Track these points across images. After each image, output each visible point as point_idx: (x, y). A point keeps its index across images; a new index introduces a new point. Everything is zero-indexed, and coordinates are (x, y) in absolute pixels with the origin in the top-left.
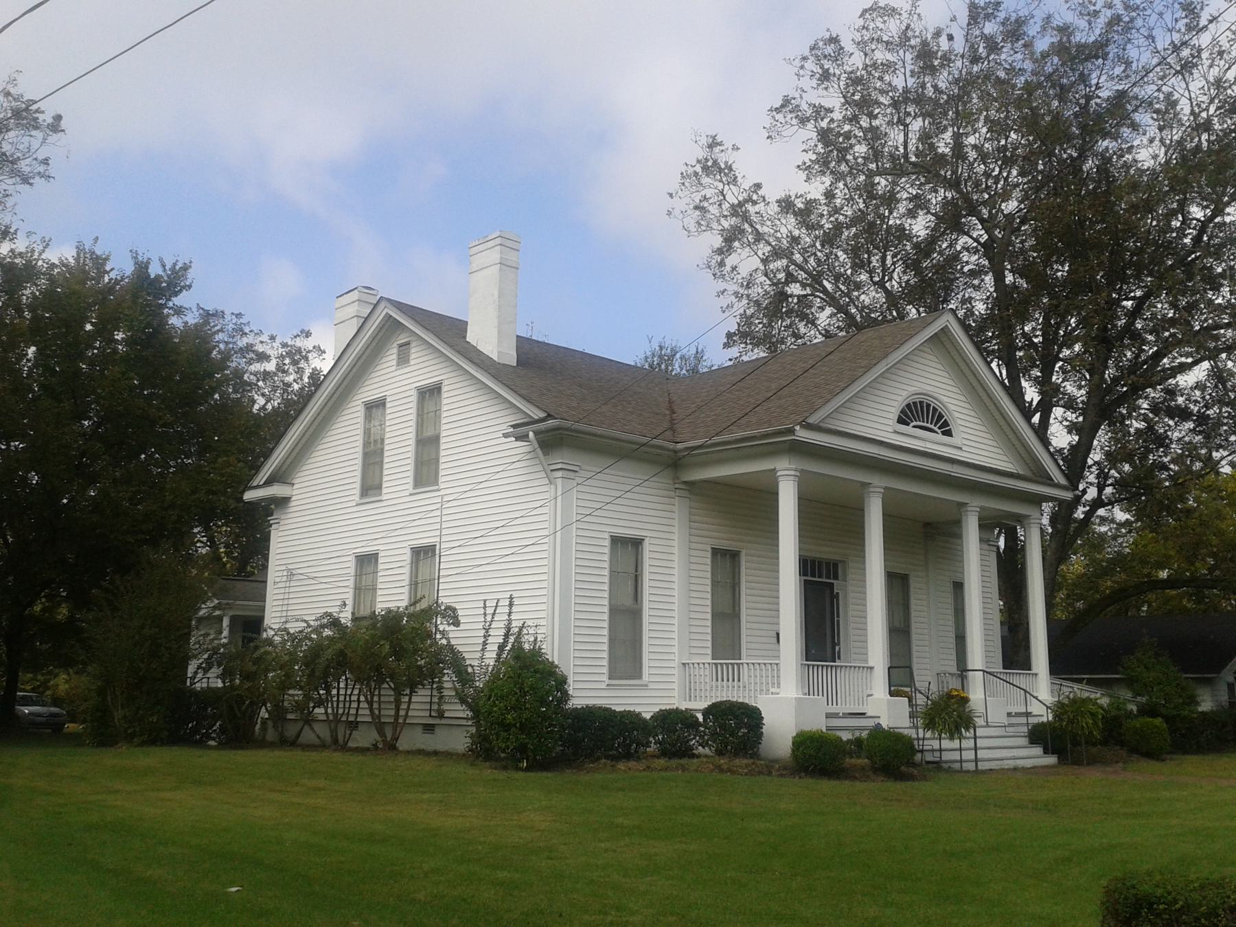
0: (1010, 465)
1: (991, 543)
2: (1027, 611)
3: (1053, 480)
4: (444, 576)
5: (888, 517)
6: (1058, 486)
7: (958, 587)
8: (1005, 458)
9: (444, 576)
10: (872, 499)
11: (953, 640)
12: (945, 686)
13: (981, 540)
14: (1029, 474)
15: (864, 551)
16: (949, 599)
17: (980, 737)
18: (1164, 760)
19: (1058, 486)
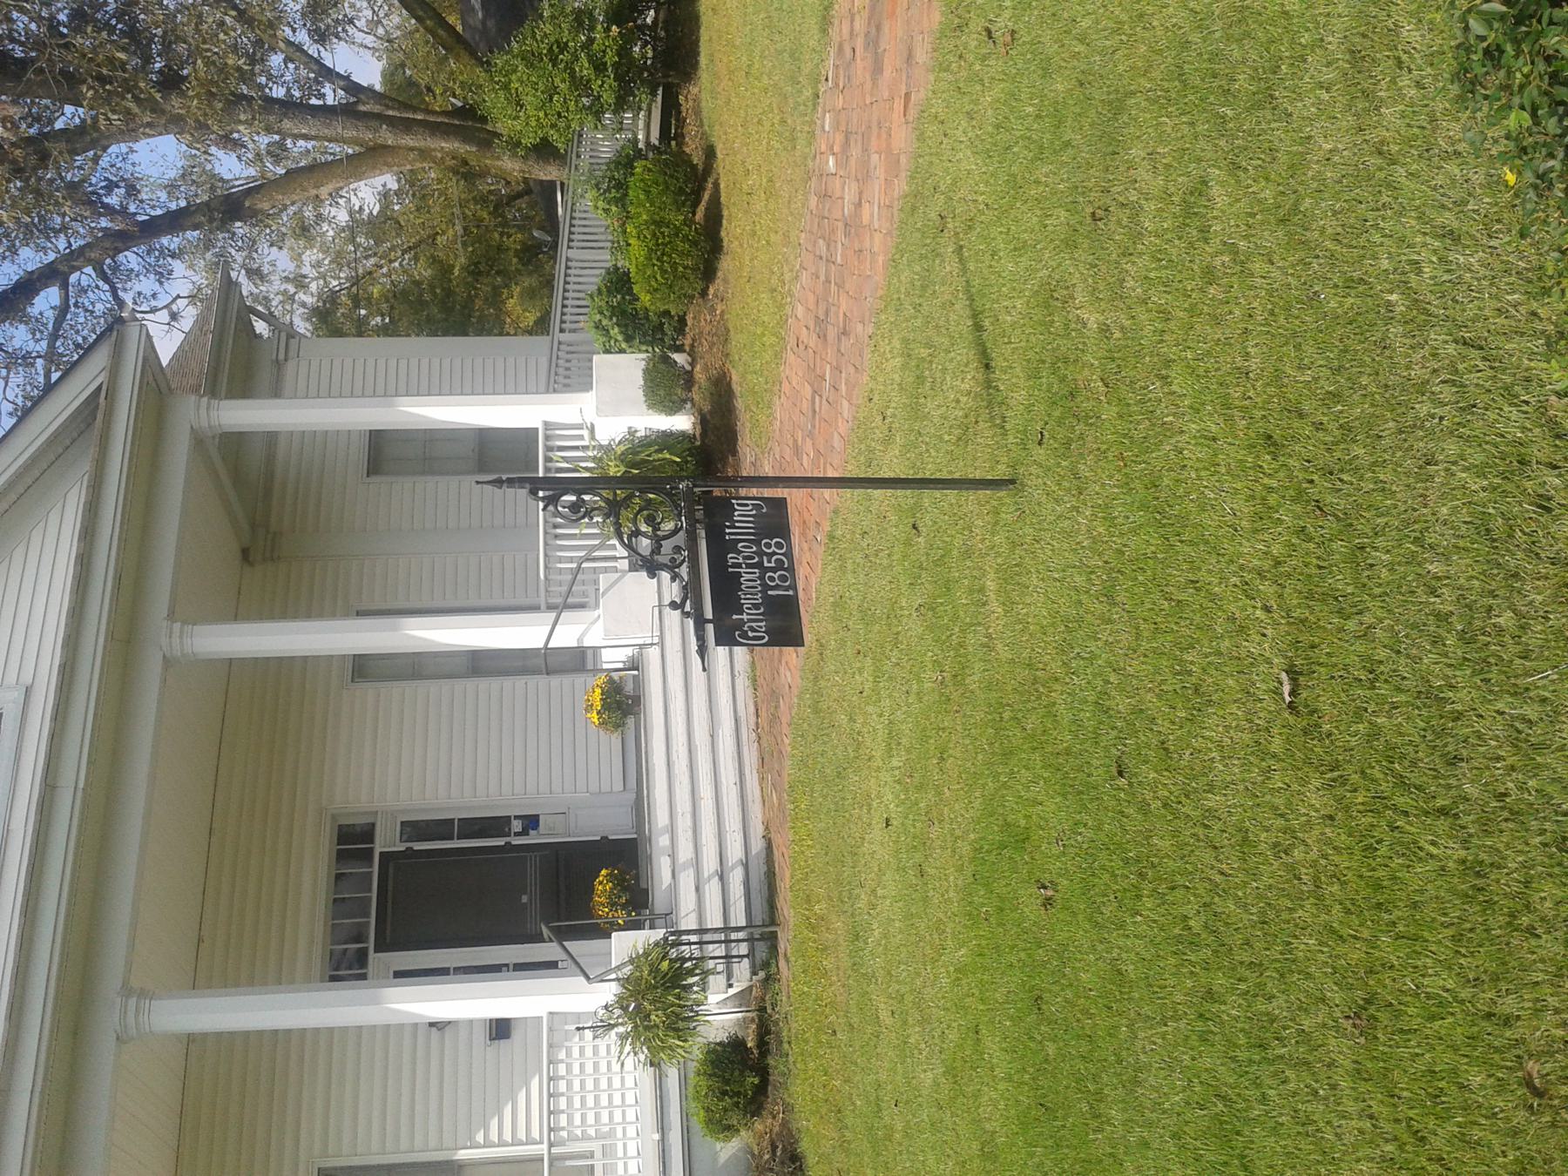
0: (75, 490)
1: (281, 356)
2: (417, 431)
3: (99, 388)
4: (500, 1134)
5: (239, 610)
6: (114, 370)
7: (362, 667)
8: (54, 518)
9: (500, 1134)
10: (223, 422)
11: (484, 684)
12: (591, 1119)
13: (276, 392)
14: (85, 467)
15: (317, 658)
16: (396, 690)
17: (700, 923)
18: (710, 153)
19: (114, 370)
